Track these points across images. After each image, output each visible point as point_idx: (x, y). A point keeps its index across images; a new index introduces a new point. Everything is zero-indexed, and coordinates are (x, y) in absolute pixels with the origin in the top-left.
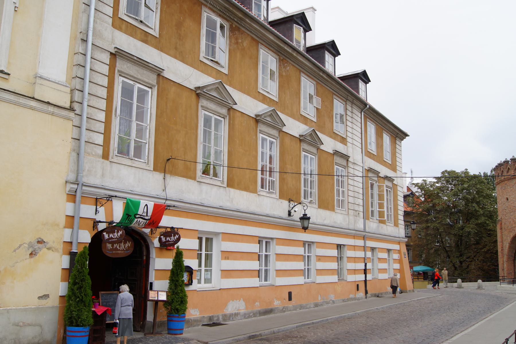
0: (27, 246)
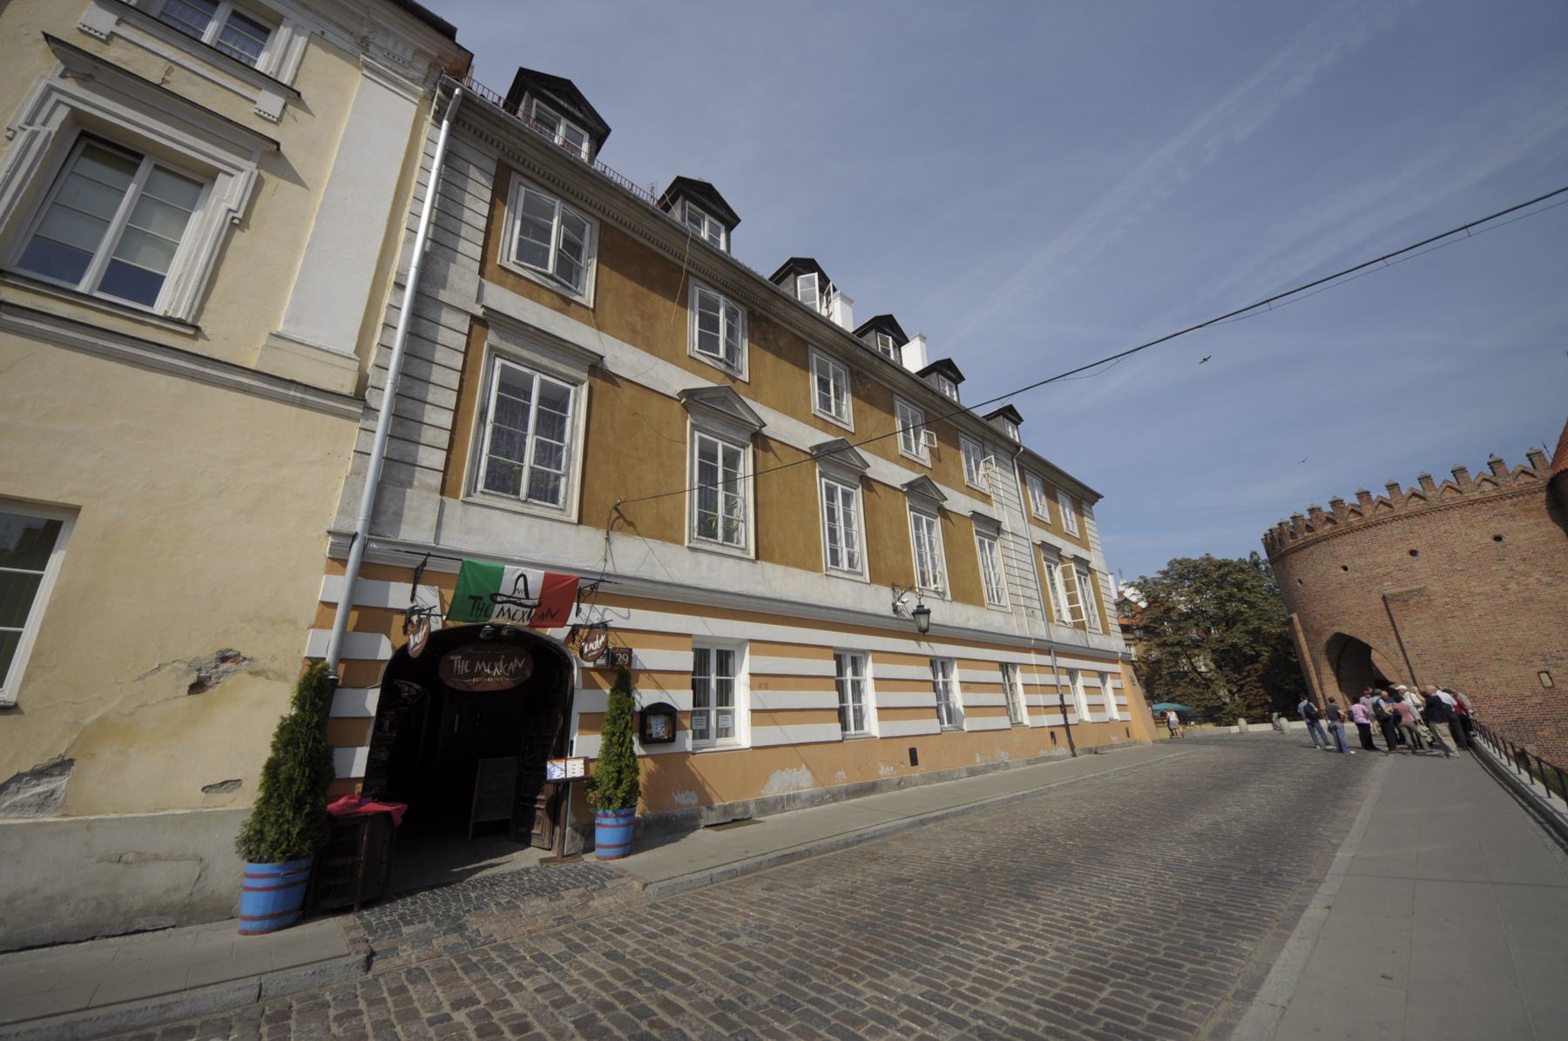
0: (184, 666)
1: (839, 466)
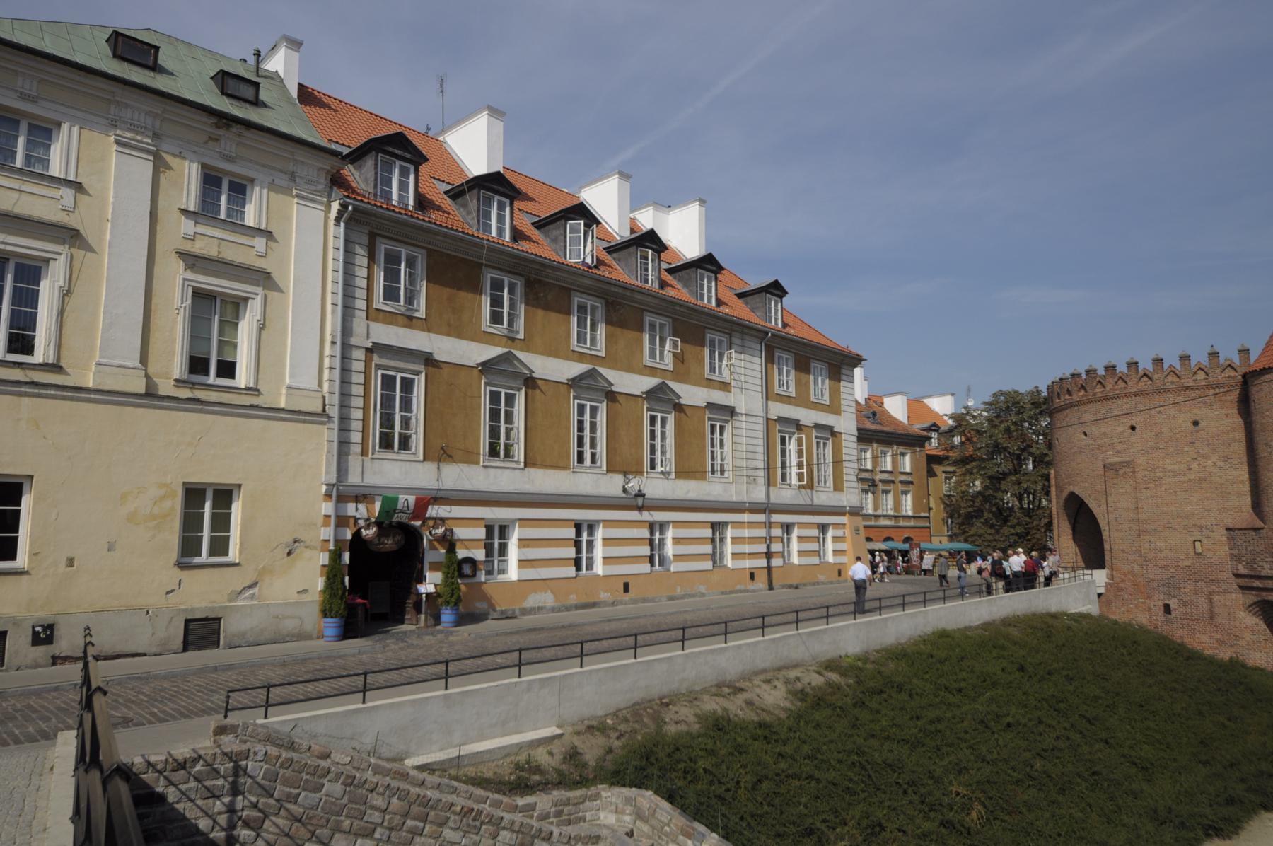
1: (589, 388)
